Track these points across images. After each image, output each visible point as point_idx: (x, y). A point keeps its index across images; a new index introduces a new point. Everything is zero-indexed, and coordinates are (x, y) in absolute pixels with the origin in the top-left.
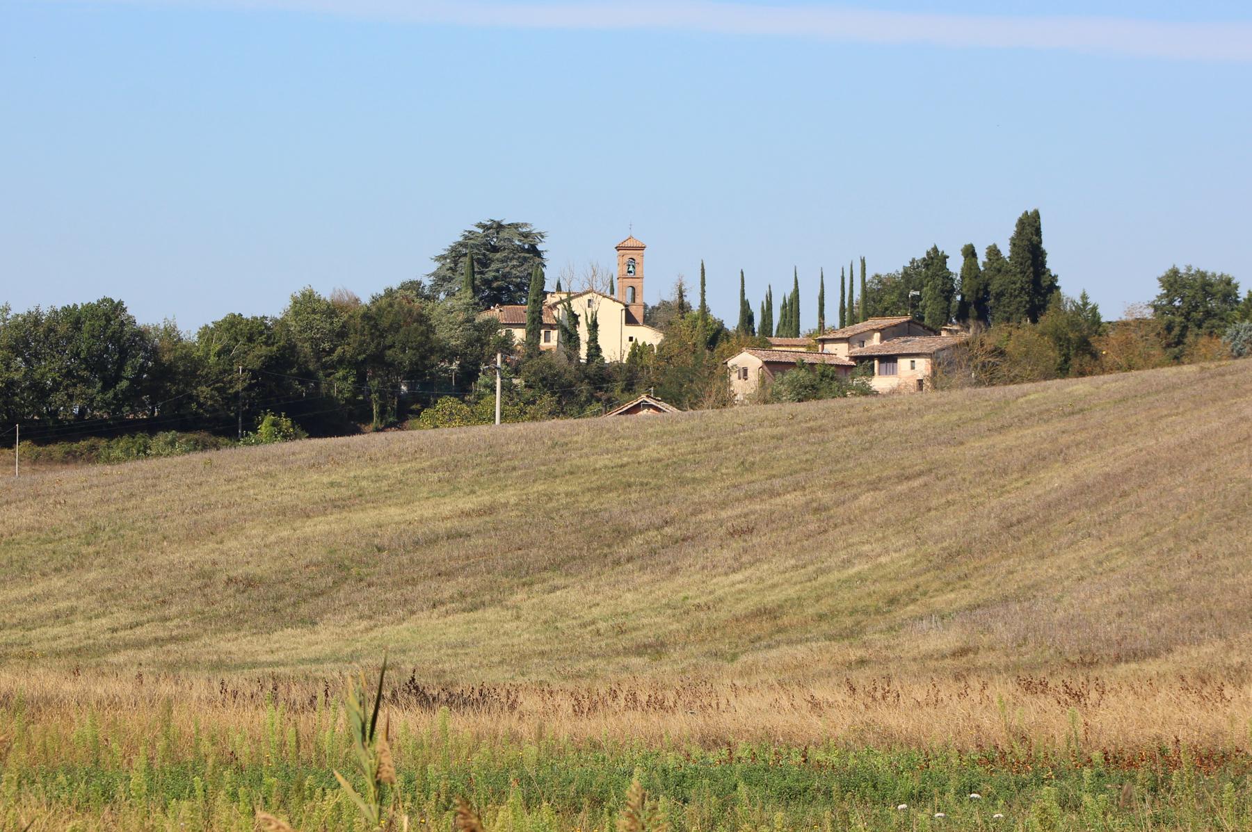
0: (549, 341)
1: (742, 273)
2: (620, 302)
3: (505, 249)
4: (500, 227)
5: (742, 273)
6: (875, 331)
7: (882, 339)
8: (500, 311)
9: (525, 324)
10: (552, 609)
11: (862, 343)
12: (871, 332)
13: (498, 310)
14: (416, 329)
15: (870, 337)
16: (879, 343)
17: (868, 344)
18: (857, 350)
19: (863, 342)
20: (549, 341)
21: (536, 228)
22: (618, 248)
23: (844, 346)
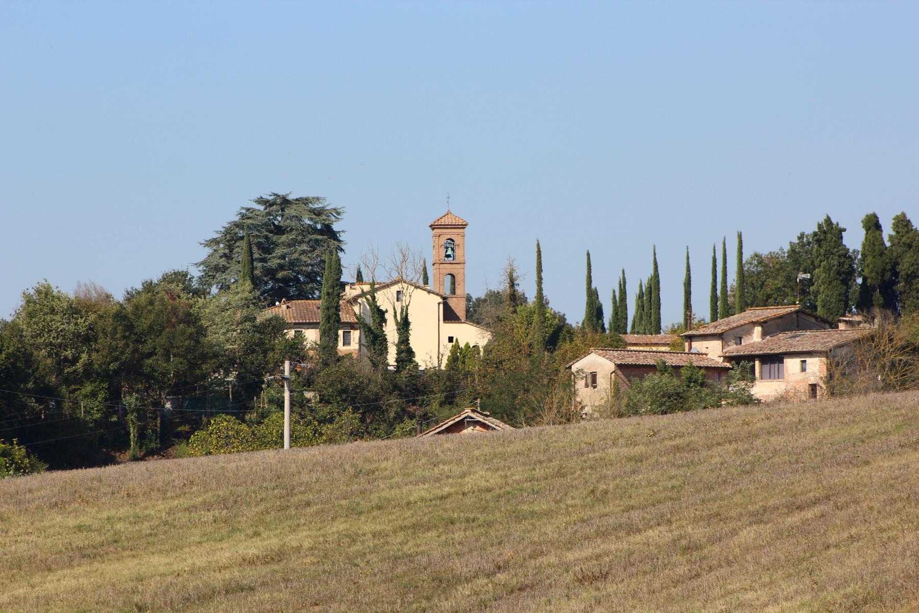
2: (437, 294)
3: (292, 230)
4: (285, 202)
7: (764, 334)
8: (288, 307)
11: (739, 340)
12: (750, 326)
13: (284, 307)
15: (749, 332)
16: (760, 340)
18: (733, 349)
21: (330, 203)
22: (433, 227)
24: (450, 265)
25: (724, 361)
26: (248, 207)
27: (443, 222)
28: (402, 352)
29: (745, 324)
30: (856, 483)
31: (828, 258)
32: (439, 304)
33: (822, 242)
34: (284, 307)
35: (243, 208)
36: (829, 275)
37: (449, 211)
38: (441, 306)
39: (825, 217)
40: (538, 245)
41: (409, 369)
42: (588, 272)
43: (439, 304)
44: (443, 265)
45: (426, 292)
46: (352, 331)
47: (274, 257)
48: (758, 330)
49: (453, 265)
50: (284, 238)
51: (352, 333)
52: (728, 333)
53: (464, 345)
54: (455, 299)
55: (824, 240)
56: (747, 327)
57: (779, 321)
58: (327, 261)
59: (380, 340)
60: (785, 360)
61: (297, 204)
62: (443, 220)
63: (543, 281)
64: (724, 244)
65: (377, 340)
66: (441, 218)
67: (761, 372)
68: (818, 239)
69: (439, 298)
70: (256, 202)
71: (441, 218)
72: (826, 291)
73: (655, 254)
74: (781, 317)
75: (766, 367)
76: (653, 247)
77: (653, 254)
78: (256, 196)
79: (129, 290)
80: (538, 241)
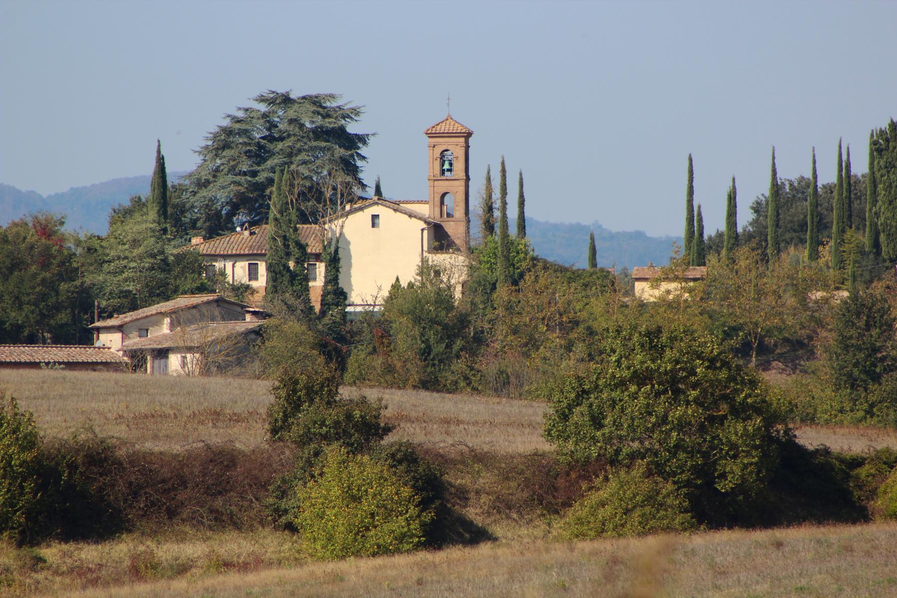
0: (256, 279)
1: (691, 160)
2: (420, 219)
3: (289, 136)
4: (286, 100)
5: (691, 160)
6: (163, 314)
7: (172, 326)
8: (252, 234)
9: (265, 255)
10: (725, 417)
11: (143, 332)
12: (160, 317)
13: (247, 233)
14: (35, 276)
15: (158, 323)
16: (169, 331)
17: (153, 333)
18: (135, 341)
19: (147, 330)
20: (256, 279)
21: (345, 100)
22: (431, 135)
23: (117, 336)
24: (447, 182)
25: (123, 355)
26: (246, 106)
27: (442, 128)
28: (329, 293)
29: (152, 315)
30: (317, 477)
31: (888, 172)
32: (423, 230)
33: (884, 152)
34: (247, 233)
35: (240, 109)
36: (890, 193)
37: (449, 116)
38: (425, 232)
39: (889, 122)
40: (503, 164)
41: (332, 316)
42: (689, 181)
43: (423, 230)
44: (440, 182)
45: (406, 217)
46: (317, 263)
47: (263, 170)
48: (167, 321)
49: (451, 182)
50: (280, 145)
51: (317, 266)
52: (129, 325)
53: (407, 284)
54: (452, 223)
55: (885, 150)
56: (154, 318)
57: (194, 311)
58: (276, 181)
59: (298, 280)
60: (170, 355)
61: (300, 103)
62: (439, 127)
63: (507, 207)
64: (848, 148)
65: (294, 279)
66: (437, 125)
67: (153, 367)
68: (878, 148)
69: (422, 223)
70: (257, 100)
71: (437, 125)
72: (886, 213)
73: (774, 158)
74: (194, 307)
75: (157, 362)
76: (772, 148)
77: (771, 158)
78: (256, 94)
79: (116, 207)
80: (503, 158)
